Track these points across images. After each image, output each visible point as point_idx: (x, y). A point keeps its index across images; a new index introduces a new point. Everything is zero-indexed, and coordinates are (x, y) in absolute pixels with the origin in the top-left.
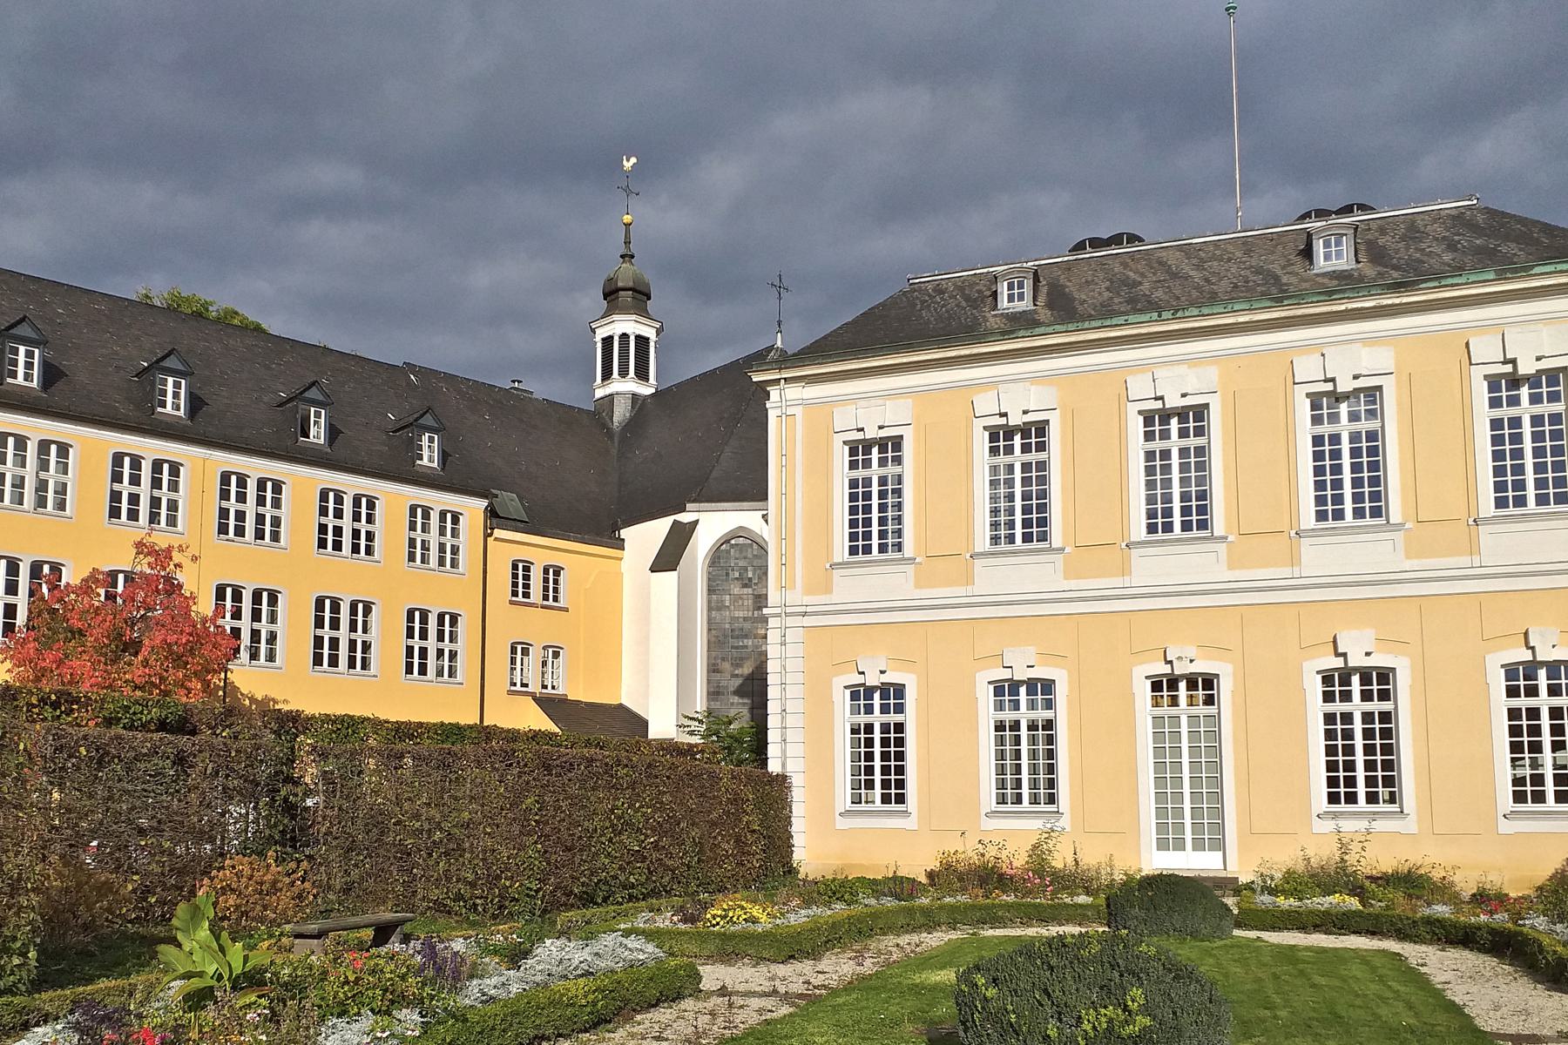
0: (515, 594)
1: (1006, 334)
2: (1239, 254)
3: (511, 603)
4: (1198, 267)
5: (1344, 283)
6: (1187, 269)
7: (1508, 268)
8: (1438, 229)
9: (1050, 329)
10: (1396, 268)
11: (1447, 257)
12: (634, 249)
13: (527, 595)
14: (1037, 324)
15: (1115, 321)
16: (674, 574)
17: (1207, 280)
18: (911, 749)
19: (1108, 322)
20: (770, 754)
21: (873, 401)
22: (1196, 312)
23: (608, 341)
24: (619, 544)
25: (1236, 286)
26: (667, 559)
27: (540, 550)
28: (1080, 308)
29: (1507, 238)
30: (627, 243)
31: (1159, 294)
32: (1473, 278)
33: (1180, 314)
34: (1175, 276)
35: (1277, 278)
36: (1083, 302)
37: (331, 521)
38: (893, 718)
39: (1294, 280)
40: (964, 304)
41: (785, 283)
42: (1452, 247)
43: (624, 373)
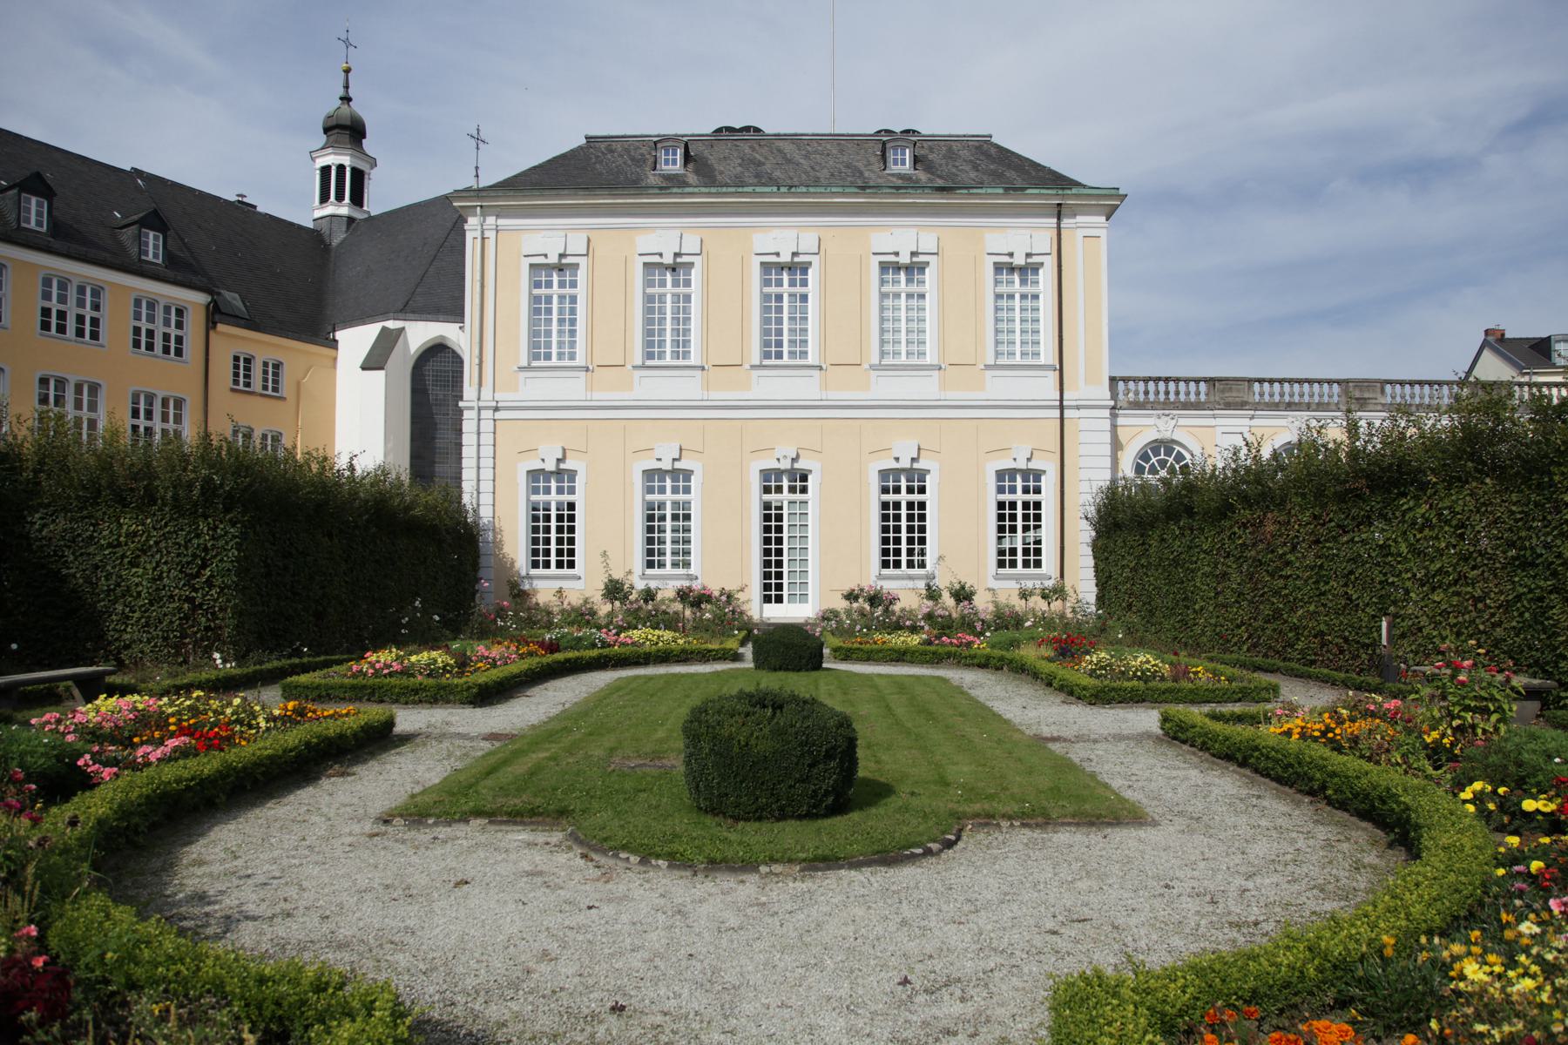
0: (236, 382)
1: (663, 190)
2: (834, 152)
3: (233, 390)
4: (806, 157)
5: (906, 185)
6: (798, 158)
7: (1010, 189)
8: (965, 153)
9: (696, 190)
10: (940, 177)
11: (973, 174)
12: (352, 93)
13: (248, 385)
14: (685, 184)
15: (746, 189)
16: (381, 374)
17: (812, 168)
18: (579, 524)
19: (740, 190)
20: (464, 477)
21: (555, 232)
22: (804, 189)
23: (325, 170)
24: (334, 344)
25: (832, 175)
26: (374, 362)
27: (263, 347)
28: (719, 177)
29: (1009, 166)
30: (347, 87)
31: (777, 174)
32: (990, 191)
33: (793, 190)
34: (789, 161)
35: (861, 173)
36: (721, 173)
37: (54, 305)
38: (566, 498)
39: (872, 175)
40: (629, 162)
41: (482, 136)
42: (976, 168)
43: (340, 197)
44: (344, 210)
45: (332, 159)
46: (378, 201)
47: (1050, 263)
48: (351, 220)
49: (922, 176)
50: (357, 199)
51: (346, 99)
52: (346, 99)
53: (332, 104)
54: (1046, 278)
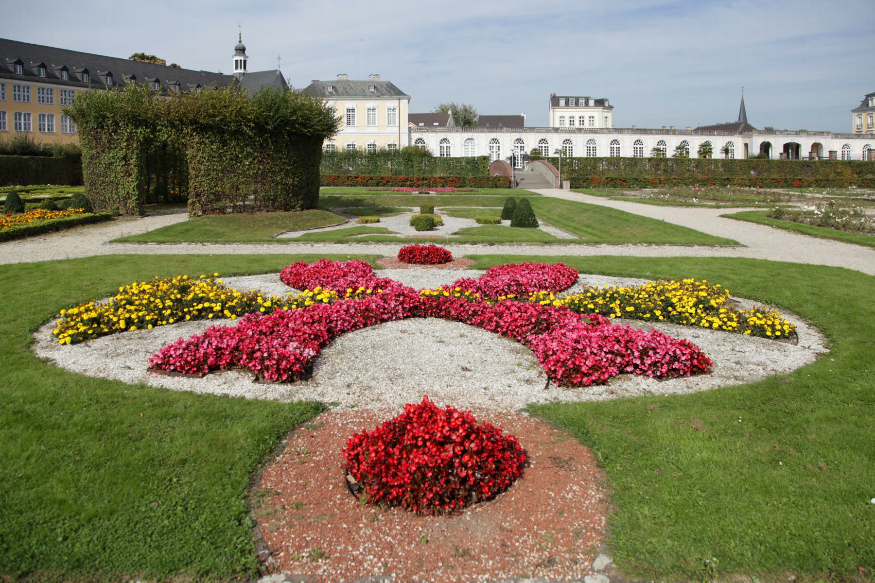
23: (237, 61)
43: (241, 68)
44: (242, 71)
45: (239, 58)
46: (250, 69)
47: (398, 109)
48: (244, 74)
49: (375, 92)
50: (245, 68)
51: (240, 41)
52: (240, 41)
53: (237, 43)
54: (397, 110)
